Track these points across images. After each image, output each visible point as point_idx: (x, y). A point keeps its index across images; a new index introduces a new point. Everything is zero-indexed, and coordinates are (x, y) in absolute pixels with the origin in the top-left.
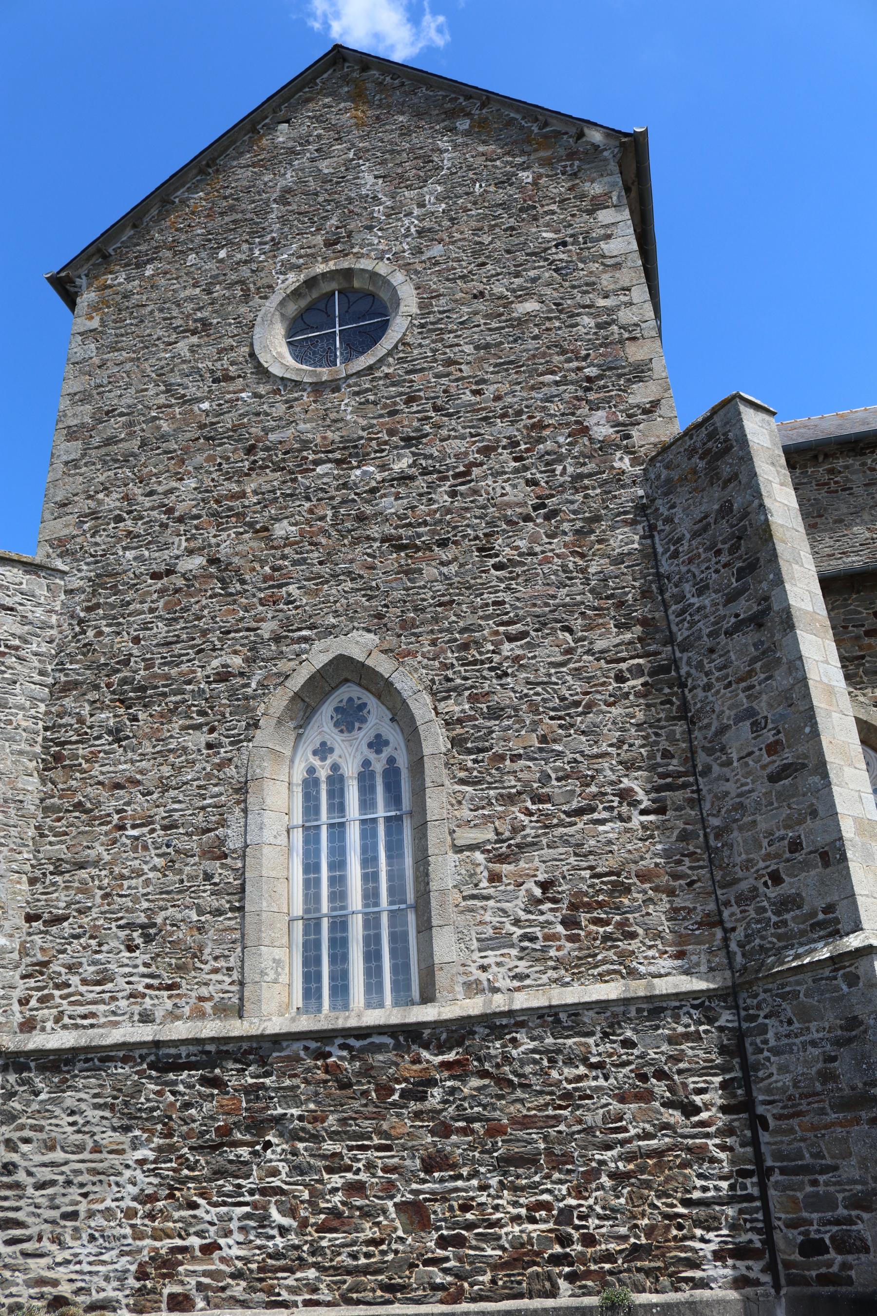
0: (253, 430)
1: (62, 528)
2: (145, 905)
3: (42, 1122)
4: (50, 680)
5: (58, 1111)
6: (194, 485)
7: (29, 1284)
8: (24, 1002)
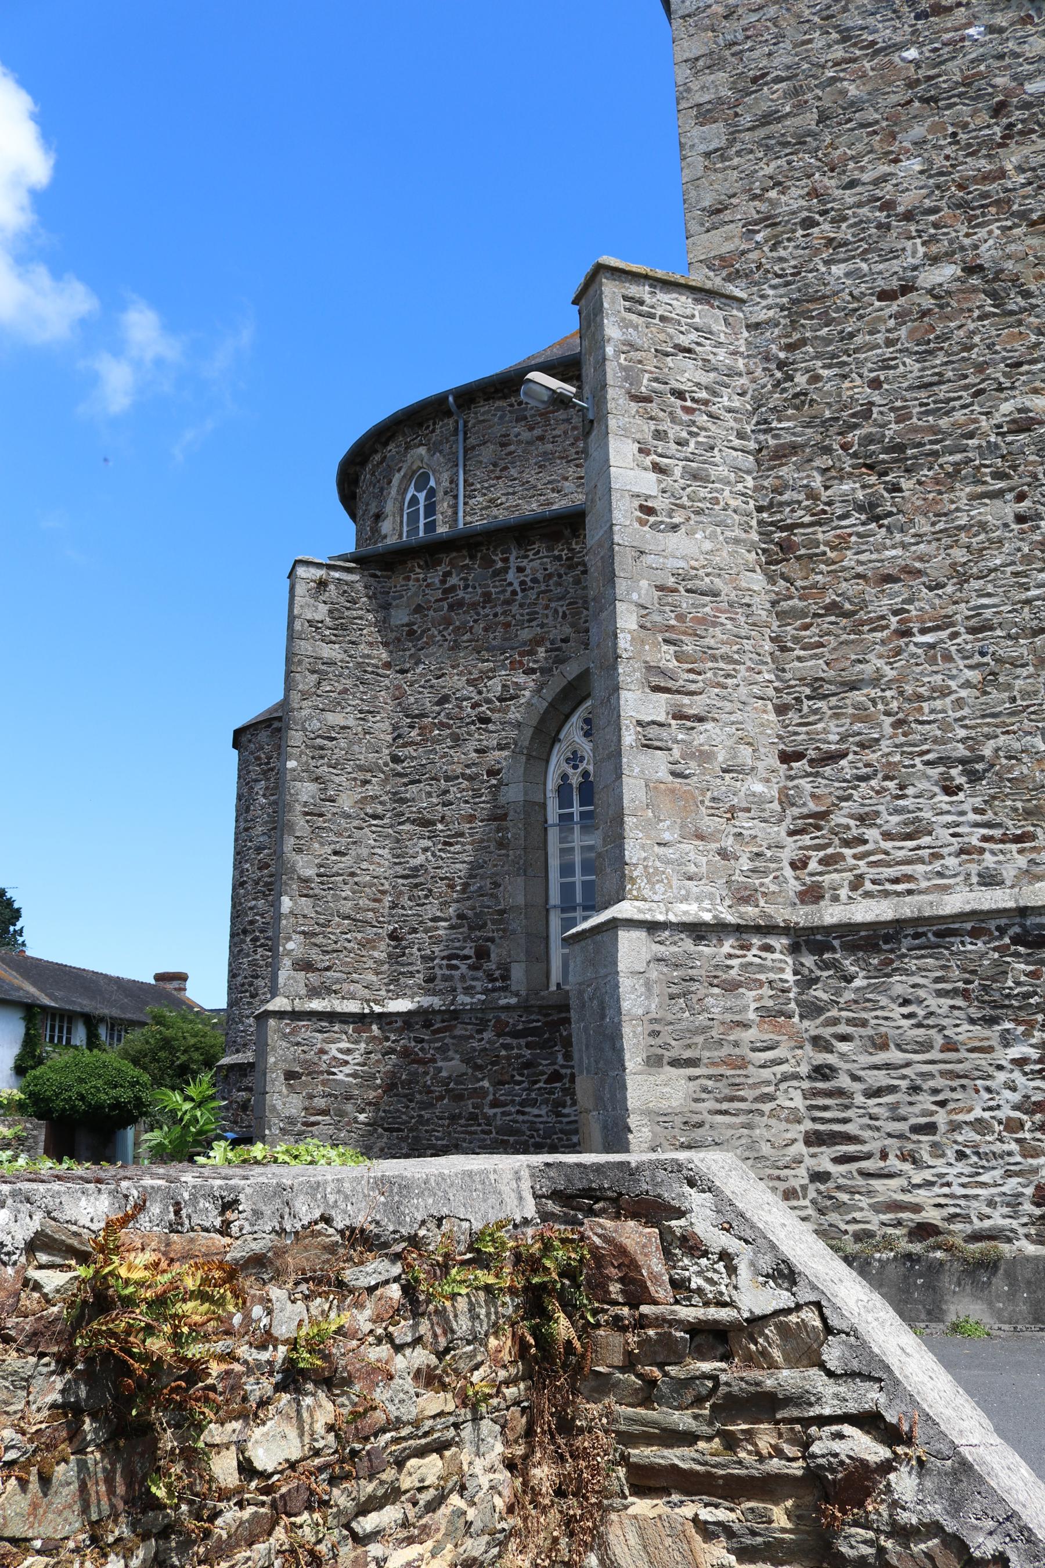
0: (998, 81)
1: (724, 241)
2: (962, 733)
3: (864, 1015)
4: (752, 445)
5: (884, 1001)
6: (918, 168)
7: (877, 1208)
8: (799, 865)
